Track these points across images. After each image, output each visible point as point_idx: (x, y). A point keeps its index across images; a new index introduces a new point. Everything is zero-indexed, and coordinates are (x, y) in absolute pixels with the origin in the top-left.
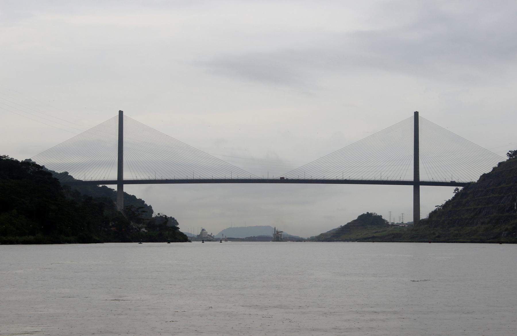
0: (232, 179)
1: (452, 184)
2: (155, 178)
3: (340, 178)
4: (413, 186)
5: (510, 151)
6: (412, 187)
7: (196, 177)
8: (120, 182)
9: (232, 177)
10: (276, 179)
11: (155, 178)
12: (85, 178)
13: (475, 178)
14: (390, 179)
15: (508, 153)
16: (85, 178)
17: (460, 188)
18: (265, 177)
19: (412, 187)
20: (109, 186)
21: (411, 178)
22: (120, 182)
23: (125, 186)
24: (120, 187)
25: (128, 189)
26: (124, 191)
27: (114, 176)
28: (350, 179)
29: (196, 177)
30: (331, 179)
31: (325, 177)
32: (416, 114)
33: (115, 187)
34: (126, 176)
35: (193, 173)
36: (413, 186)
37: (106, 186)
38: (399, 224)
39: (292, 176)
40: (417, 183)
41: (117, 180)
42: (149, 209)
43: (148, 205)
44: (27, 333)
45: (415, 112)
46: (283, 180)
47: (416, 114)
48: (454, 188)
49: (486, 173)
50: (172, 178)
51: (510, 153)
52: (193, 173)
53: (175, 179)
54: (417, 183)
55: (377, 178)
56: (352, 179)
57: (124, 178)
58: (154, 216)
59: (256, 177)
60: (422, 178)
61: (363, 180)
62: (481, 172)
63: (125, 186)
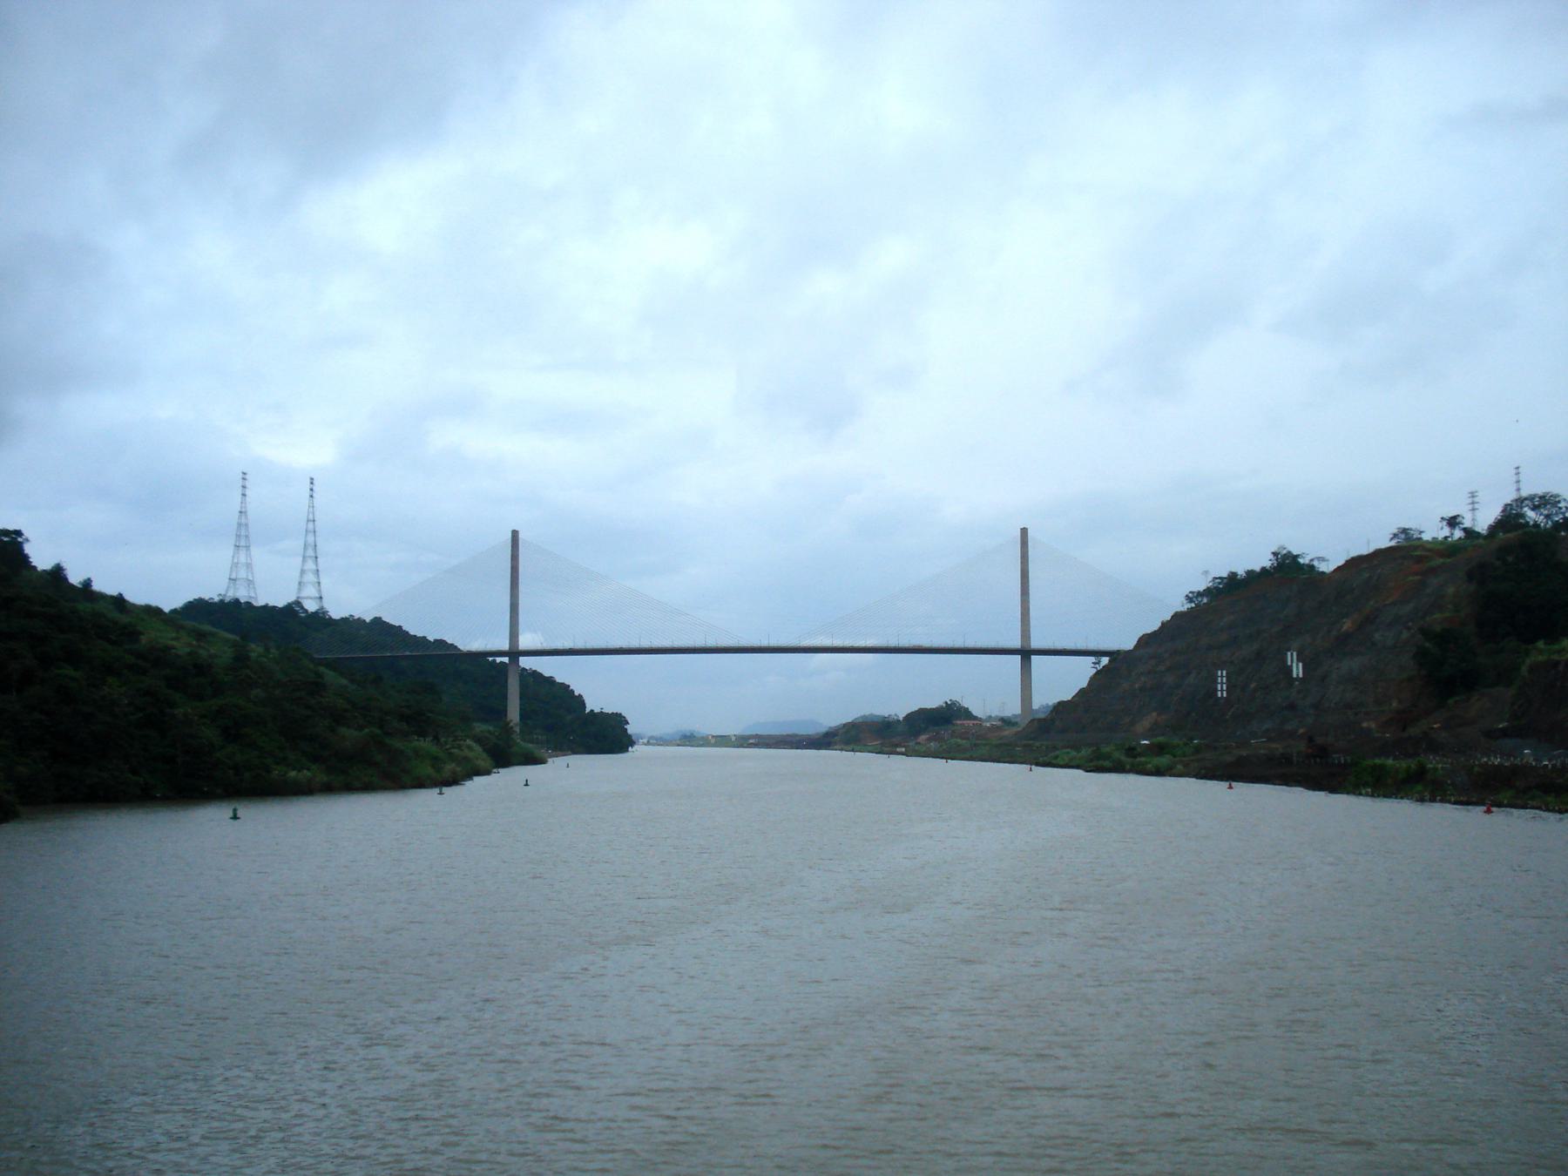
1: (1098, 654)
4: (1020, 656)
5: (1190, 592)
6: (1019, 657)
12: (1518, 490)
13: (1128, 643)
15: (1187, 596)
16: (1518, 490)
17: (1105, 660)
18: (765, 643)
19: (1019, 657)
20: (499, 660)
21: (1016, 643)
22: (515, 654)
23: (522, 659)
25: (526, 662)
27: (505, 646)
32: (1024, 531)
34: (526, 641)
36: (1020, 656)
38: (554, 756)
40: (1026, 654)
42: (580, 701)
43: (576, 694)
44: (904, 1006)
46: (689, 739)
47: (1024, 531)
48: (1093, 659)
51: (1190, 595)
54: (1026, 654)
57: (520, 643)
63: (522, 659)
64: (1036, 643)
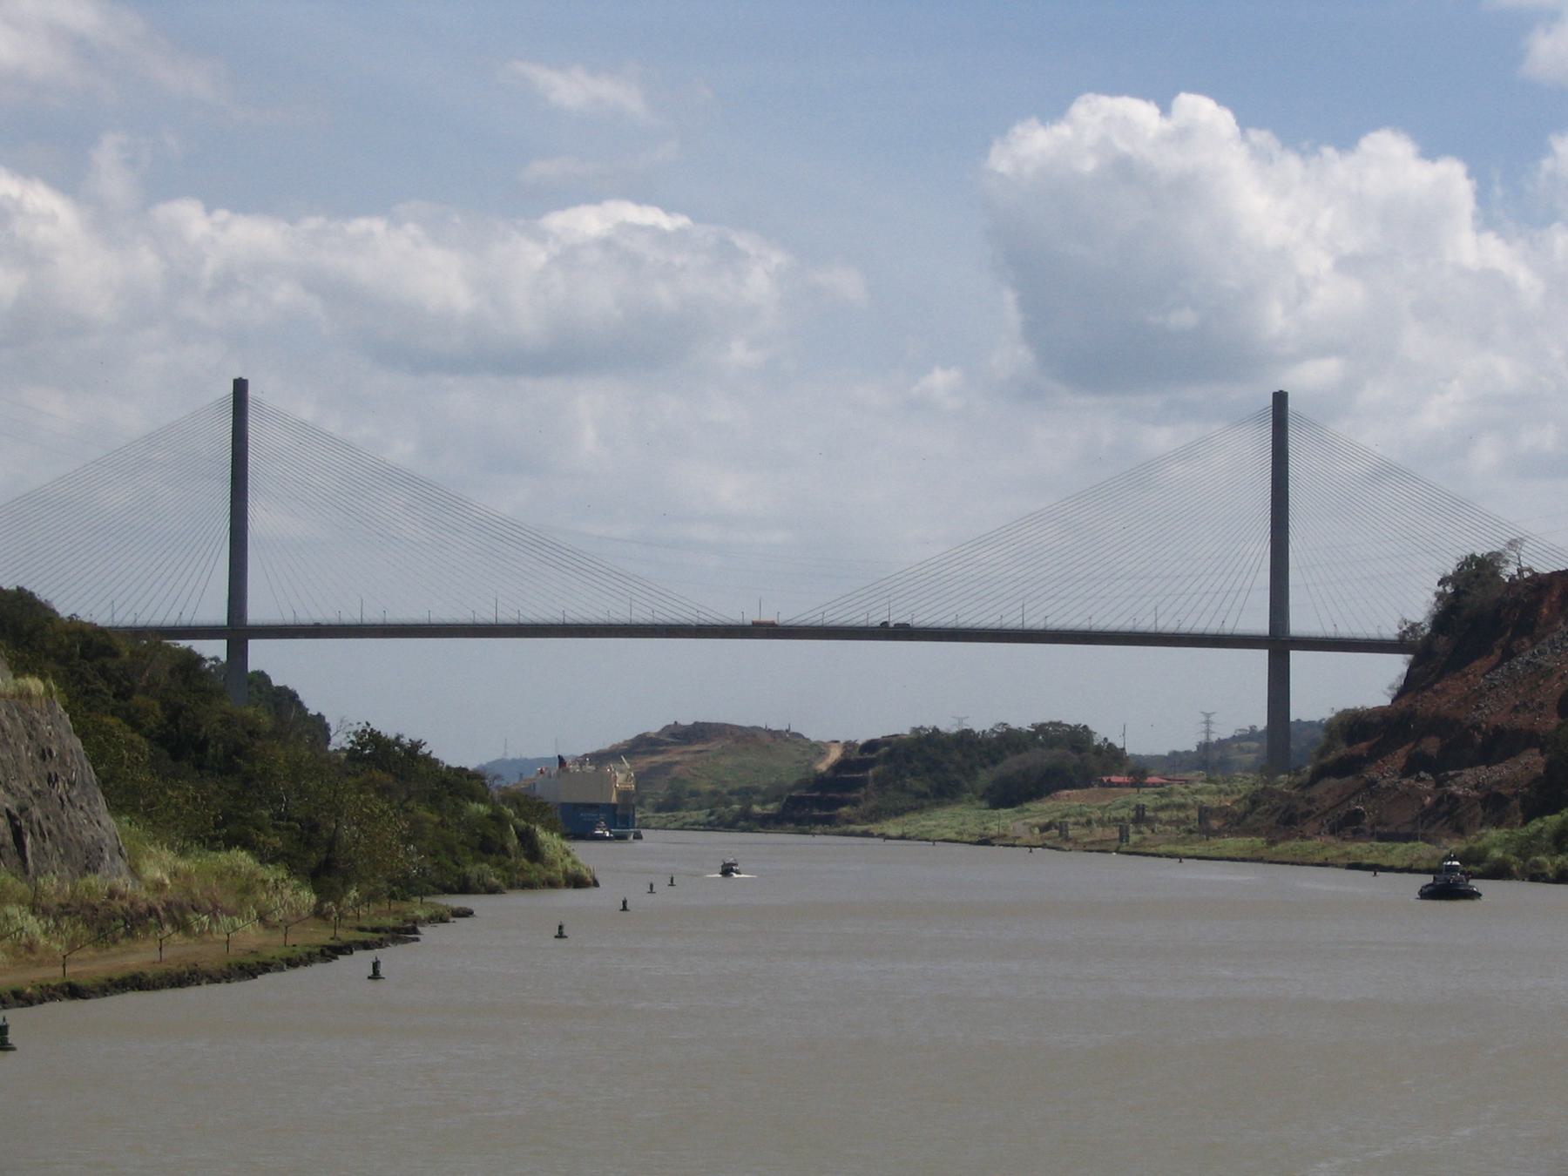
0: (634, 625)
2: (362, 619)
3: (486, 616)
6: (1263, 655)
7: (680, 618)
8: (238, 632)
9: (499, 616)
10: (789, 623)
11: (362, 619)
12: (113, 615)
14: (1345, 631)
16: (113, 615)
19: (1263, 655)
22: (238, 632)
24: (238, 652)
25: (262, 656)
26: (253, 665)
28: (1048, 628)
29: (680, 618)
30: (835, 623)
31: (959, 620)
32: (240, 386)
33: (214, 650)
35: (631, 599)
37: (189, 650)
39: (941, 616)
41: (1267, 633)
45: (1287, 393)
49: (1547, 572)
50: (536, 618)
52: (631, 599)
53: (521, 622)
55: (1113, 625)
56: (1009, 627)
58: (331, 748)
59: (718, 617)
60: (256, 613)
61: (1094, 628)
62: (1504, 538)
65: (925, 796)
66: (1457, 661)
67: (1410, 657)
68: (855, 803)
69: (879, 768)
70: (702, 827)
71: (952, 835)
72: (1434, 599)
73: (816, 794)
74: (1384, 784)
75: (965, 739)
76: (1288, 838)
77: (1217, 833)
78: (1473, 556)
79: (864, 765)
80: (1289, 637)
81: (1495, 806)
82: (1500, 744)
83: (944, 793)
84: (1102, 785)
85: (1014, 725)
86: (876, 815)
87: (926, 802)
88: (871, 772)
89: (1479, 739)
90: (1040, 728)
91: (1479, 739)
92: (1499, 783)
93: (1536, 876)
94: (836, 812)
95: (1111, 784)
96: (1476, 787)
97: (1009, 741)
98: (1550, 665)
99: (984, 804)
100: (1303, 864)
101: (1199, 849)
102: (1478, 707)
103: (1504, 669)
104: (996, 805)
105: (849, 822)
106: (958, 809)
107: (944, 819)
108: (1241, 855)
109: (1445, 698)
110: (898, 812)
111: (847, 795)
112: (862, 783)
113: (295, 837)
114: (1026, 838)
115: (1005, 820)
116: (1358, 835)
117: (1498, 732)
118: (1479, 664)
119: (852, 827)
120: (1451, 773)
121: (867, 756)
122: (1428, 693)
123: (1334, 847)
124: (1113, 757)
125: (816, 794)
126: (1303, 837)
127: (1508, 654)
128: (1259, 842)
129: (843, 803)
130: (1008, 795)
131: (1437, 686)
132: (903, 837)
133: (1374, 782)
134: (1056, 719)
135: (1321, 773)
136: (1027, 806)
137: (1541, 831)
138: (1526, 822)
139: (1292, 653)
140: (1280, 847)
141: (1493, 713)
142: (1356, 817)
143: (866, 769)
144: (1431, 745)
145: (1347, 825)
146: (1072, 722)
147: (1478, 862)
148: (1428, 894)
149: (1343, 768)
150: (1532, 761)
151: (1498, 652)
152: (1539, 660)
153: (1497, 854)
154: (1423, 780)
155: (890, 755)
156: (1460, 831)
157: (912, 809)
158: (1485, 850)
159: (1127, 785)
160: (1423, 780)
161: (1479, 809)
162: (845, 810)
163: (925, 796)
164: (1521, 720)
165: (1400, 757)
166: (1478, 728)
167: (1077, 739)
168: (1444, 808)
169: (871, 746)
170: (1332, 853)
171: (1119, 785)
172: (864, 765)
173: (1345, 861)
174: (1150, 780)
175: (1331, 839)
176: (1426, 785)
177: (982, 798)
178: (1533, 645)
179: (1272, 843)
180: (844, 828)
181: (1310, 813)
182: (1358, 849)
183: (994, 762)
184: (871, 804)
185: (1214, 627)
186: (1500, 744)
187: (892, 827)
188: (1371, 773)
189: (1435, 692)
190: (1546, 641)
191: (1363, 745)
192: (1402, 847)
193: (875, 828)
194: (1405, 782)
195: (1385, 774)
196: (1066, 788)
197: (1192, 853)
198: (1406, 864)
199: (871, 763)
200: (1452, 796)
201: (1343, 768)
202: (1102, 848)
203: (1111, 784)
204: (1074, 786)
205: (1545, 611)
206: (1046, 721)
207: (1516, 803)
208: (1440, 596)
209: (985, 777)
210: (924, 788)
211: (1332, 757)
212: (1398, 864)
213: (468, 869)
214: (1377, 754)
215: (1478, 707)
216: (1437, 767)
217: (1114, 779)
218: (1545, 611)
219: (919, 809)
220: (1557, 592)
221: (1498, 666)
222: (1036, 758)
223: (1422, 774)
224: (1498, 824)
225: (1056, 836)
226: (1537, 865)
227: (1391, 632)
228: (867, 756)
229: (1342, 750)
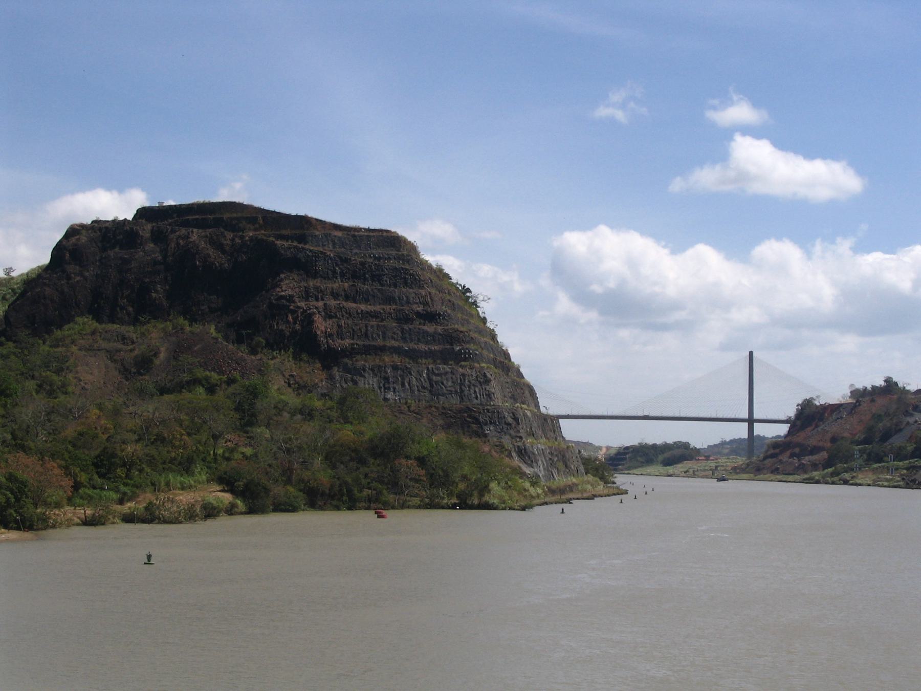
6: (746, 424)
14: (769, 417)
19: (746, 424)
54: (751, 421)
64: (756, 416)
65: (643, 463)
66: (803, 427)
67: (789, 425)
68: (623, 465)
69: (630, 455)
70: (886, 484)
71: (657, 474)
72: (796, 411)
73: (611, 462)
74: (784, 460)
75: (654, 446)
76: (760, 474)
77: (739, 473)
78: (806, 399)
79: (625, 454)
80: (817, 407)
81: (815, 466)
82: (815, 450)
83: (649, 461)
84: (696, 460)
85: (668, 442)
86: (629, 468)
87: (643, 464)
88: (627, 456)
89: (809, 449)
90: (675, 443)
91: (809, 449)
92: (815, 460)
93: (827, 483)
94: (617, 468)
95: (699, 460)
96: (809, 461)
97: (666, 447)
98: (828, 429)
99: (662, 465)
100: (766, 481)
101: (734, 477)
102: (809, 441)
103: (816, 430)
104: (665, 465)
105: (622, 470)
106: (654, 466)
107: (650, 469)
108: (748, 479)
109: (800, 438)
110: (636, 468)
111: (620, 463)
112: (625, 459)
113: (76, 495)
114: (681, 475)
115: (670, 470)
116: (779, 474)
117: (815, 447)
118: (809, 429)
119: (623, 472)
120: (802, 458)
121: (626, 451)
122: (795, 436)
123: (773, 477)
124: (697, 451)
125: (611, 462)
126: (764, 474)
127: (817, 426)
128: (752, 475)
129: (620, 465)
130: (668, 463)
131: (798, 435)
132: (642, 474)
133: (781, 460)
134: (680, 440)
135: (765, 458)
136: (675, 466)
137: (827, 472)
138: (823, 470)
139: (755, 424)
140: (757, 477)
141: (813, 442)
142: (777, 469)
143: (626, 455)
144: (797, 450)
145: (775, 471)
146: (684, 441)
147: (812, 480)
148: (717, 481)
149: (772, 456)
150: (824, 455)
151: (814, 426)
152: (825, 428)
153: (817, 478)
154: (794, 459)
155: (633, 452)
156: (806, 472)
157: (640, 467)
158: (814, 477)
159: (704, 460)
160: (794, 459)
161: (810, 467)
162: (620, 467)
163: (643, 463)
164: (821, 444)
165: (788, 453)
166: (809, 446)
167: (686, 446)
168: (801, 466)
169: (627, 448)
170: (772, 478)
171: (701, 460)
172: (625, 454)
173: (776, 480)
174: (711, 458)
175: (772, 475)
176: (796, 461)
177: (661, 463)
178: (823, 424)
179: (756, 476)
180: (621, 472)
181: (764, 468)
182: (779, 477)
183: (663, 453)
184: (628, 465)
185: (733, 416)
186: (815, 450)
187: (635, 471)
188: (780, 457)
189: (797, 436)
190: (827, 423)
191: (778, 450)
192: (792, 476)
193: (630, 472)
194: (790, 460)
195: (785, 457)
196: (685, 461)
197: (736, 478)
198: (794, 480)
199: (628, 453)
200: (803, 464)
201: (772, 456)
202: (706, 477)
203: (699, 460)
204: (687, 460)
205: (826, 415)
206: (677, 441)
207: (820, 465)
208: (797, 410)
209: (661, 458)
210: (644, 461)
211: (769, 453)
212: (792, 481)
213: (471, 333)
214: (781, 452)
215: (809, 441)
216: (799, 456)
217: (700, 458)
218: (826, 415)
219: (642, 466)
220: (829, 410)
221: (814, 429)
222: (677, 452)
223: (795, 458)
224: (816, 470)
225: (686, 474)
226: (828, 480)
227: (783, 418)
228: (626, 451)
229: (771, 451)
